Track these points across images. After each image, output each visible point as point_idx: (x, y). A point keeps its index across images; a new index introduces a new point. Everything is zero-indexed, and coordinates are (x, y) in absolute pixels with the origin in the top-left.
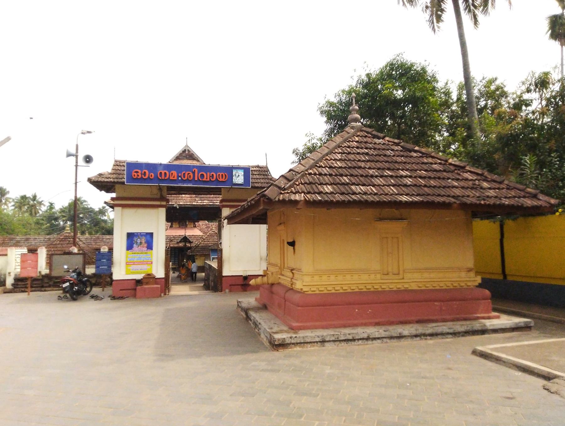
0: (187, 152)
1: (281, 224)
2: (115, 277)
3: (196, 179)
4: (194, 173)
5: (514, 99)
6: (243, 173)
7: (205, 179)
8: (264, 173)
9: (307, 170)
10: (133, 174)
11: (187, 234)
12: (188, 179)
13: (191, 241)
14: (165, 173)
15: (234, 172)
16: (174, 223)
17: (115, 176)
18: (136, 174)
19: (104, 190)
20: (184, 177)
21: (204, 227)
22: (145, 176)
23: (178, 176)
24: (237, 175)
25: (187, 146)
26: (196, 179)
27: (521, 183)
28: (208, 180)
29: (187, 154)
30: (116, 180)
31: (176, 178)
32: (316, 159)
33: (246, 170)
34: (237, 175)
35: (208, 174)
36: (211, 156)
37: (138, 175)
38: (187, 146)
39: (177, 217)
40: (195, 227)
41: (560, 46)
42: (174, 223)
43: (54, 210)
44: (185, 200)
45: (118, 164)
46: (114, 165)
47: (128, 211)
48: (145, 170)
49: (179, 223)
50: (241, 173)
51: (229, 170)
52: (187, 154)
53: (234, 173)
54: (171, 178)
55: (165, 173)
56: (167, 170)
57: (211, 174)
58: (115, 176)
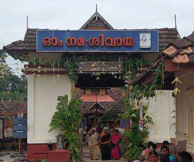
0: (97, 19)
1: (188, 89)
2: (29, 142)
3: (103, 45)
6: (150, 37)
8: (172, 36)
12: (58, 44)
13: (103, 107)
14: (73, 39)
15: (141, 35)
16: (86, 90)
17: (26, 44)
20: (91, 43)
21: (116, 94)
22: (119, 44)
24: (144, 39)
25: (97, 13)
29: (97, 21)
30: (27, 48)
33: (153, 32)
34: (144, 39)
36: (120, 20)
37: (48, 43)
38: (97, 13)
39: (85, 82)
40: (107, 93)
42: (86, 90)
43: (63, 133)
44: (96, 68)
45: (30, 32)
46: (26, 34)
48: (54, 38)
49: (92, 90)
51: (136, 33)
52: (97, 21)
53: (141, 37)
55: (73, 39)
56: (75, 37)
58: (26, 44)
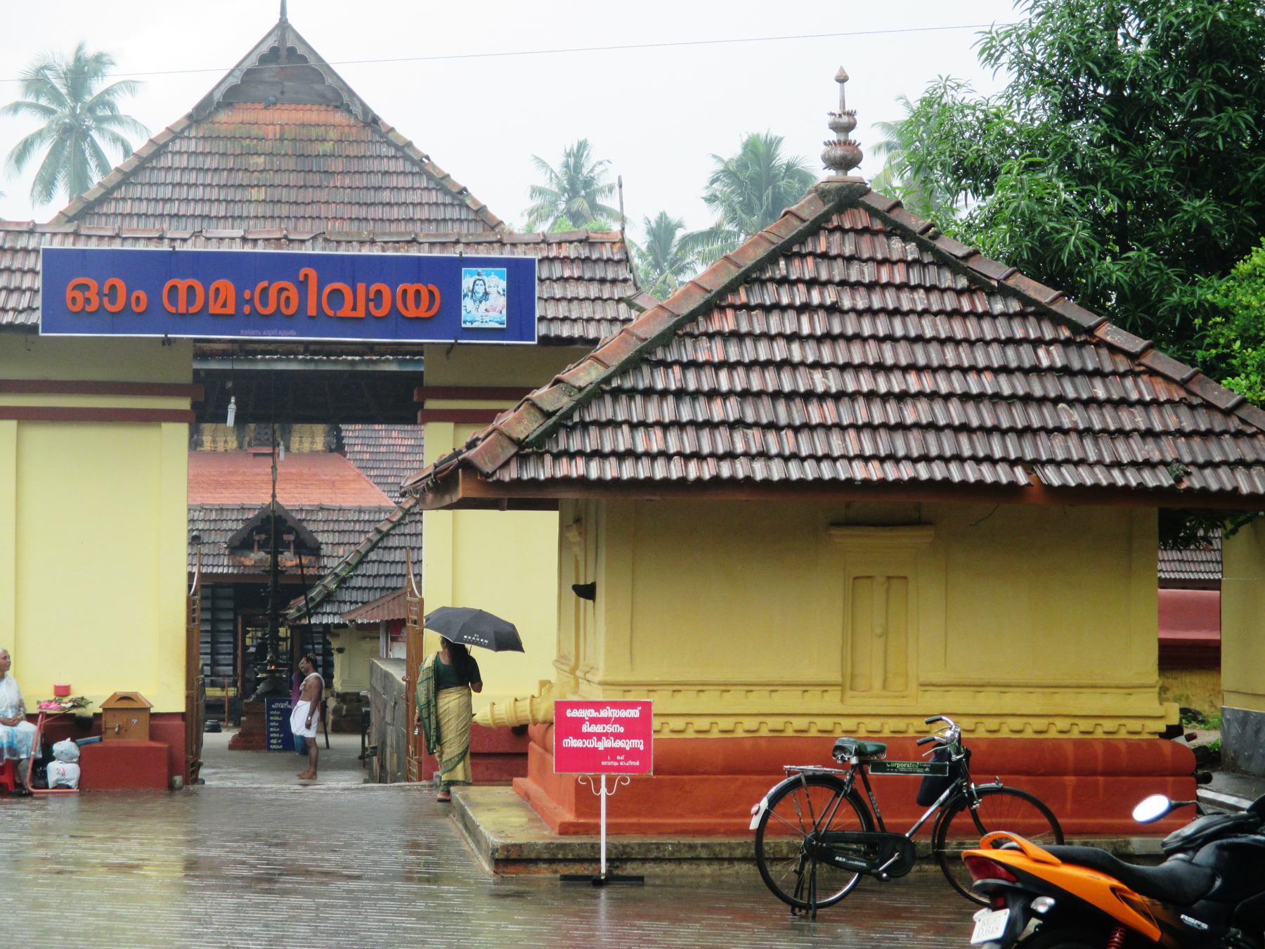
3: (312, 311)
4: (303, 285)
5: (1084, 228)
6: (503, 284)
7: (346, 311)
9: (607, 380)
10: (69, 294)
11: (292, 498)
18: (77, 294)
19: (487, 212)
20: (264, 303)
23: (240, 301)
24: (480, 290)
25: (283, 26)
26: (312, 311)
27: (1078, 202)
28: (361, 313)
31: (230, 309)
32: (716, 289)
34: (480, 290)
35: (361, 287)
37: (88, 300)
38: (283, 26)
41: (292, 19)
47: (42, 437)
50: (497, 282)
53: (467, 282)
54: (214, 309)
57: (374, 287)
